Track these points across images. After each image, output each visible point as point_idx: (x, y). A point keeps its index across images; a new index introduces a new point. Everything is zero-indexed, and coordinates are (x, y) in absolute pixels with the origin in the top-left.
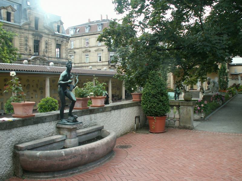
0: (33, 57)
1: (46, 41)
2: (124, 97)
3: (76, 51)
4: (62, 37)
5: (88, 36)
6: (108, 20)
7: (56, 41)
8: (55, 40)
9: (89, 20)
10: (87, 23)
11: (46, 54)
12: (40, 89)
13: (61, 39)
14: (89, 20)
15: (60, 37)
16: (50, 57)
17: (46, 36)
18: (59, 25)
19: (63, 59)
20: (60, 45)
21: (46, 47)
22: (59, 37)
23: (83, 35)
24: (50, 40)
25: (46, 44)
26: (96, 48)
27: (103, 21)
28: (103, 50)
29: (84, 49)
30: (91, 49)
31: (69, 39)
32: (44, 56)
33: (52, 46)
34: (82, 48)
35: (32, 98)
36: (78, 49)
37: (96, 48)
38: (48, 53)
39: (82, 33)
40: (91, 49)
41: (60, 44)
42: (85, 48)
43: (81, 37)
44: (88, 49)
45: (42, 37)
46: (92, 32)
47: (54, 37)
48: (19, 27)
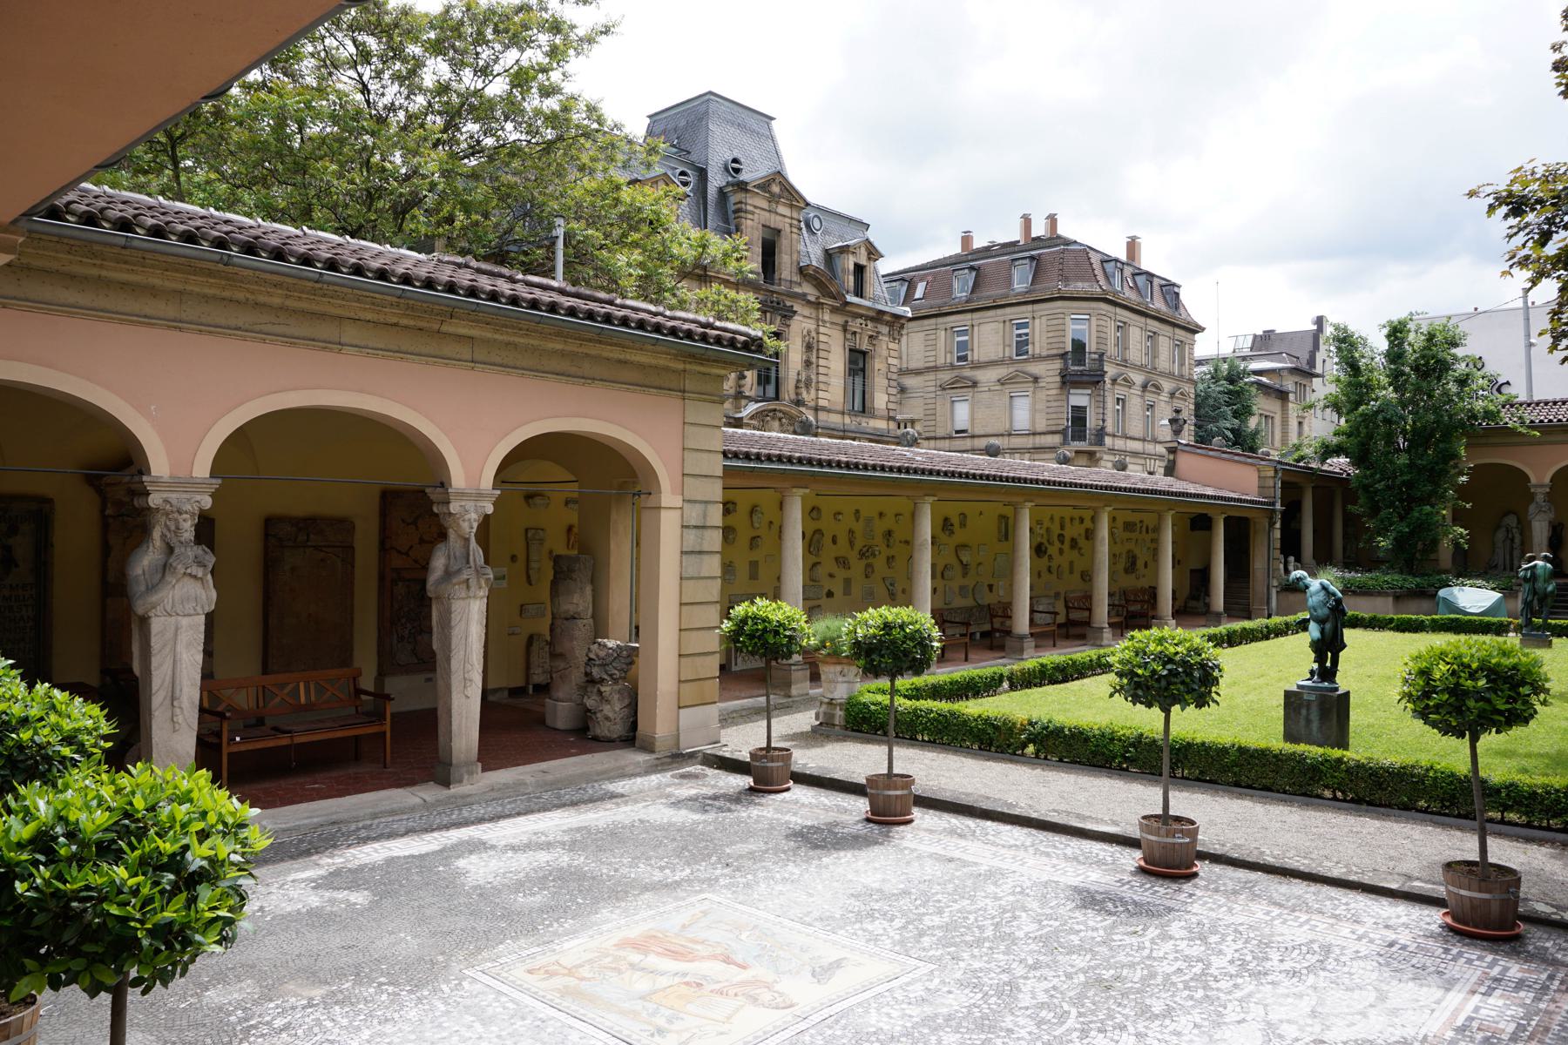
0: (753, 407)
1: (809, 332)
2: (1218, 601)
3: (910, 382)
4: (872, 319)
5: (969, 316)
6: (1059, 237)
8: (845, 330)
9: (1132, 246)
10: (957, 256)
11: (805, 395)
12: (862, 555)
14: (966, 239)
15: (867, 318)
16: (824, 409)
17: (807, 311)
18: (863, 261)
19: (874, 417)
20: (864, 353)
21: (808, 363)
22: (861, 316)
23: (946, 309)
25: (809, 347)
26: (1001, 372)
27: (1036, 244)
28: (1036, 379)
29: (946, 376)
30: (980, 375)
31: (902, 327)
32: (799, 403)
33: (831, 356)
34: (935, 369)
35: (830, 594)
36: (918, 372)
37: (1001, 372)
38: (813, 391)
39: (939, 302)
40: (980, 375)
41: (864, 348)
42: (952, 367)
43: (933, 321)
44: (967, 373)
45: (790, 318)
46: (988, 297)
47: (840, 319)
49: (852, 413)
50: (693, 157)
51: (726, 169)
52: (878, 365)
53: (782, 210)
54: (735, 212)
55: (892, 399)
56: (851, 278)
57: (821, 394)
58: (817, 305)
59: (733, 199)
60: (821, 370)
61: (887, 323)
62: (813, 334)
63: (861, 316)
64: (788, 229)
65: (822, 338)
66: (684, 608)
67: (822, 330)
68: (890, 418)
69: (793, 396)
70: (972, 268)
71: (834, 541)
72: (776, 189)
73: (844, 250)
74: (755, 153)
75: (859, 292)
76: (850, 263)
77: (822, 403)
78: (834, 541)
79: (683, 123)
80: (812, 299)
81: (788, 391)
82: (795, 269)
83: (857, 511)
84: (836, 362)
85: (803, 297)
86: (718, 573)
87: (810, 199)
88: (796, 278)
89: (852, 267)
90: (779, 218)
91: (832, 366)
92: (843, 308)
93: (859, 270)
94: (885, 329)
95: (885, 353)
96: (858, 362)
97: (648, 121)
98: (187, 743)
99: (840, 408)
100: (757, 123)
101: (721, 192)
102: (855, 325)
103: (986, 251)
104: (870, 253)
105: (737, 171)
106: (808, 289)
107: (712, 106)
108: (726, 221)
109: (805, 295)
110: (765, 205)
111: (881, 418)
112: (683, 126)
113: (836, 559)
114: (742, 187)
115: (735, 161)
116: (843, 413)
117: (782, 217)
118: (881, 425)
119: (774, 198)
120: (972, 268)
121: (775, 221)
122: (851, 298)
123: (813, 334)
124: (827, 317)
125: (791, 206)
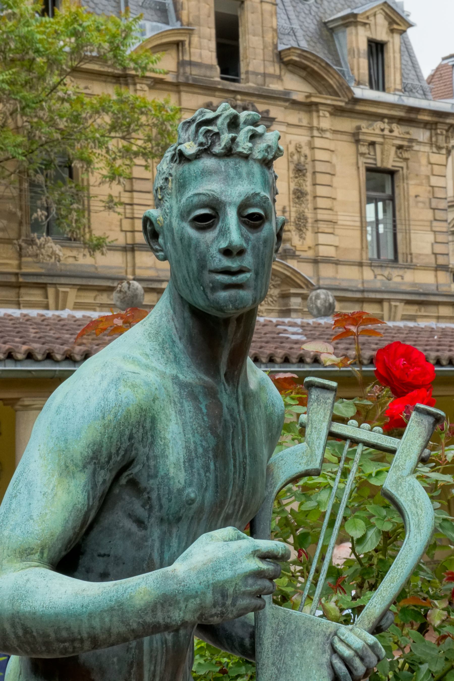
4: (400, 121)
7: (364, 149)
8: (357, 142)
13: (398, 130)
16: (328, 260)
17: (294, 117)
18: (381, 34)
19: (411, 267)
20: (392, 173)
22: (381, 117)
24: (318, 143)
33: (336, 181)
38: (309, 235)
41: (389, 164)
47: (348, 125)
48: (402, 114)
49: (377, 263)
52: (412, 190)
55: (441, 238)
56: (364, 63)
57: (322, 238)
58: (309, 107)
60: (321, 203)
61: (426, 125)
62: (306, 150)
63: (381, 117)
65: (320, 155)
66: (445, 163)
67: (318, 143)
68: (439, 268)
73: (351, 21)
75: (377, 81)
76: (358, 39)
77: (324, 251)
80: (299, 97)
84: (345, 185)
85: (284, 99)
86: (91, 188)
89: (363, 46)
91: (340, 195)
92: (351, 108)
93: (377, 49)
94: (422, 135)
95: (424, 170)
96: (381, 182)
98: (397, 440)
99: (355, 257)
102: (372, 130)
104: (392, 22)
109: (287, 92)
111: (425, 268)
116: (361, 264)
118: (426, 279)
122: (363, 92)
123: (306, 150)
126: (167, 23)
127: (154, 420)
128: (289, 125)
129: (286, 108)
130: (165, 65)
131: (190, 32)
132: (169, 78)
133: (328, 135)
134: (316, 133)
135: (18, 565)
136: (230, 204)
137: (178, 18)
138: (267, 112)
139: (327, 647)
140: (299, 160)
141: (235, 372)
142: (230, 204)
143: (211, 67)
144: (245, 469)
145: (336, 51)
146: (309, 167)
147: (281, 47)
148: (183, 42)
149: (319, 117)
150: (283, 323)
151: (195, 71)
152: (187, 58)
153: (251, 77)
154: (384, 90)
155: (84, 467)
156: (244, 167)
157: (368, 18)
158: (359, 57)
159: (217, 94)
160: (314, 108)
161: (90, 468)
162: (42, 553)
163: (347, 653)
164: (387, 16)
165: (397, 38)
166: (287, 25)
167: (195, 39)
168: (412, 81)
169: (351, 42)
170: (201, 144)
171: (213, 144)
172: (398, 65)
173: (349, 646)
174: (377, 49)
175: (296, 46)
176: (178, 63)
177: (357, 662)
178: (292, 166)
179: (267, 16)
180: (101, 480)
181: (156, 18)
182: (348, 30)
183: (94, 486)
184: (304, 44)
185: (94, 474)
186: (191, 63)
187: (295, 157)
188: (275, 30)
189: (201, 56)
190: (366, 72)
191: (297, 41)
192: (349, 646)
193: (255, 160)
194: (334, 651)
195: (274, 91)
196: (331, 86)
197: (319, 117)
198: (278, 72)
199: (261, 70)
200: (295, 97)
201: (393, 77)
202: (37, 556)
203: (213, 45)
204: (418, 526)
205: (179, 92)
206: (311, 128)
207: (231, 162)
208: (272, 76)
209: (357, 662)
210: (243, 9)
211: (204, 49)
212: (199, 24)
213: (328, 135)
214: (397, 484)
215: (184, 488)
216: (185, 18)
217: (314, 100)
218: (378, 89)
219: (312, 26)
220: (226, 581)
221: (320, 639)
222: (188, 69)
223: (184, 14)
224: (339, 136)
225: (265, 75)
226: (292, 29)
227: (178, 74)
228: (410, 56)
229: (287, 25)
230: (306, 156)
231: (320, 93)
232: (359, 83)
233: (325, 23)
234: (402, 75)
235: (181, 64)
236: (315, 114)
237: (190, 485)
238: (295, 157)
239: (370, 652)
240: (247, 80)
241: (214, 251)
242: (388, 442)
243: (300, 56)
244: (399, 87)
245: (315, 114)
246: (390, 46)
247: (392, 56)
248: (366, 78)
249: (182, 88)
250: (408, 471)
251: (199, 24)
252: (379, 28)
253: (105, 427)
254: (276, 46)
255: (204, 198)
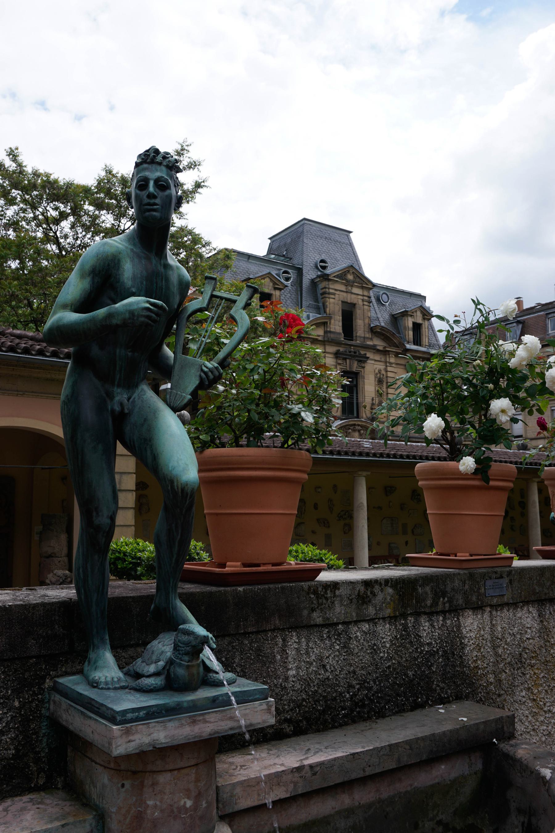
1: (380, 371)
14: (519, 303)
17: (377, 357)
18: (419, 320)
24: (389, 369)
25: (380, 382)
41: (354, 369)
45: (365, 362)
50: (296, 261)
51: (317, 267)
53: (355, 290)
54: (322, 294)
56: (411, 333)
58: (385, 352)
59: (321, 286)
62: (383, 372)
64: (360, 302)
65: (390, 374)
67: (389, 369)
69: (369, 415)
70: (519, 322)
71: (316, 507)
72: (350, 277)
73: (405, 314)
74: (338, 255)
75: (417, 341)
76: (409, 322)
78: (316, 507)
79: (289, 241)
80: (381, 348)
81: (365, 413)
82: (367, 330)
83: (335, 486)
85: (374, 349)
87: (375, 280)
88: (368, 335)
89: (411, 325)
90: (353, 296)
93: (417, 327)
97: (269, 241)
100: (340, 237)
101: (314, 283)
103: (531, 310)
105: (324, 268)
106: (379, 343)
107: (306, 228)
108: (316, 300)
109: (375, 346)
110: (343, 288)
112: (290, 242)
113: (318, 520)
114: (325, 277)
115: (322, 261)
117: (356, 295)
119: (349, 284)
120: (519, 322)
121: (350, 298)
123: (383, 372)
124: (392, 360)
125: (362, 288)
126: (320, 314)
127: (119, 261)
128: (375, 361)
129: (374, 353)
130: (319, 332)
131: (330, 318)
132: (320, 338)
133: (394, 365)
134: (388, 365)
135: (62, 311)
136: (151, 179)
137: (325, 312)
138: (365, 354)
139: (200, 369)
140: (380, 376)
141: (161, 253)
142: (151, 179)
143: (340, 334)
144: (162, 290)
145: (398, 327)
146: (385, 380)
147: (372, 325)
148: (327, 322)
149: (389, 357)
150: (363, 441)
151: (332, 336)
152: (329, 330)
153: (358, 338)
154: (420, 346)
155: (89, 275)
156: (158, 167)
157: (413, 313)
158: (408, 330)
159: (343, 346)
160: (387, 353)
161: (92, 275)
162: (71, 307)
163: (205, 369)
164: (422, 312)
165: (426, 322)
166: (375, 316)
167: (332, 321)
168: (433, 341)
169: (405, 323)
170: (143, 159)
171: (147, 159)
172: (427, 334)
173: (207, 368)
174: (417, 327)
175: (379, 324)
176: (325, 332)
177: (210, 374)
178: (377, 379)
179: (365, 311)
180: (96, 281)
181: (315, 312)
182: (404, 318)
183: (93, 283)
184: (383, 324)
185: (93, 278)
186: (330, 332)
187: (378, 375)
188: (369, 318)
189: (335, 328)
190: (412, 337)
191: (380, 323)
192: (207, 368)
193: (164, 165)
194: (202, 370)
195: (369, 345)
196: (395, 343)
197: (389, 357)
198: (370, 337)
199: (363, 336)
200: (378, 348)
201: (425, 341)
202: (69, 308)
203: (341, 324)
204: (242, 327)
205: (325, 345)
206: (386, 362)
207: (154, 165)
208: (368, 338)
209: (210, 374)
210: (355, 308)
211: (336, 326)
212: (334, 314)
213: (394, 365)
214: (236, 312)
215: (130, 288)
216: (328, 312)
217: (387, 349)
218: (417, 345)
219: (387, 317)
220: (134, 310)
221: (198, 366)
222: (329, 335)
223: (328, 310)
224: (399, 366)
225: (364, 338)
226: (377, 317)
227: (324, 337)
228: (433, 331)
229: (375, 316)
230: (383, 375)
231: (390, 346)
232: (408, 343)
233: (393, 315)
234: (429, 339)
235: (326, 332)
236: (388, 356)
237: (134, 287)
238: (378, 375)
239: (215, 370)
240: (356, 340)
241: (145, 197)
242: (234, 297)
243: (381, 329)
244: (427, 344)
245: (388, 356)
246: (423, 325)
247: (425, 330)
248: (412, 340)
249: (326, 343)
250: (241, 307)
251: (334, 314)
252: (418, 318)
253: (98, 260)
254: (370, 325)
255: (142, 178)
